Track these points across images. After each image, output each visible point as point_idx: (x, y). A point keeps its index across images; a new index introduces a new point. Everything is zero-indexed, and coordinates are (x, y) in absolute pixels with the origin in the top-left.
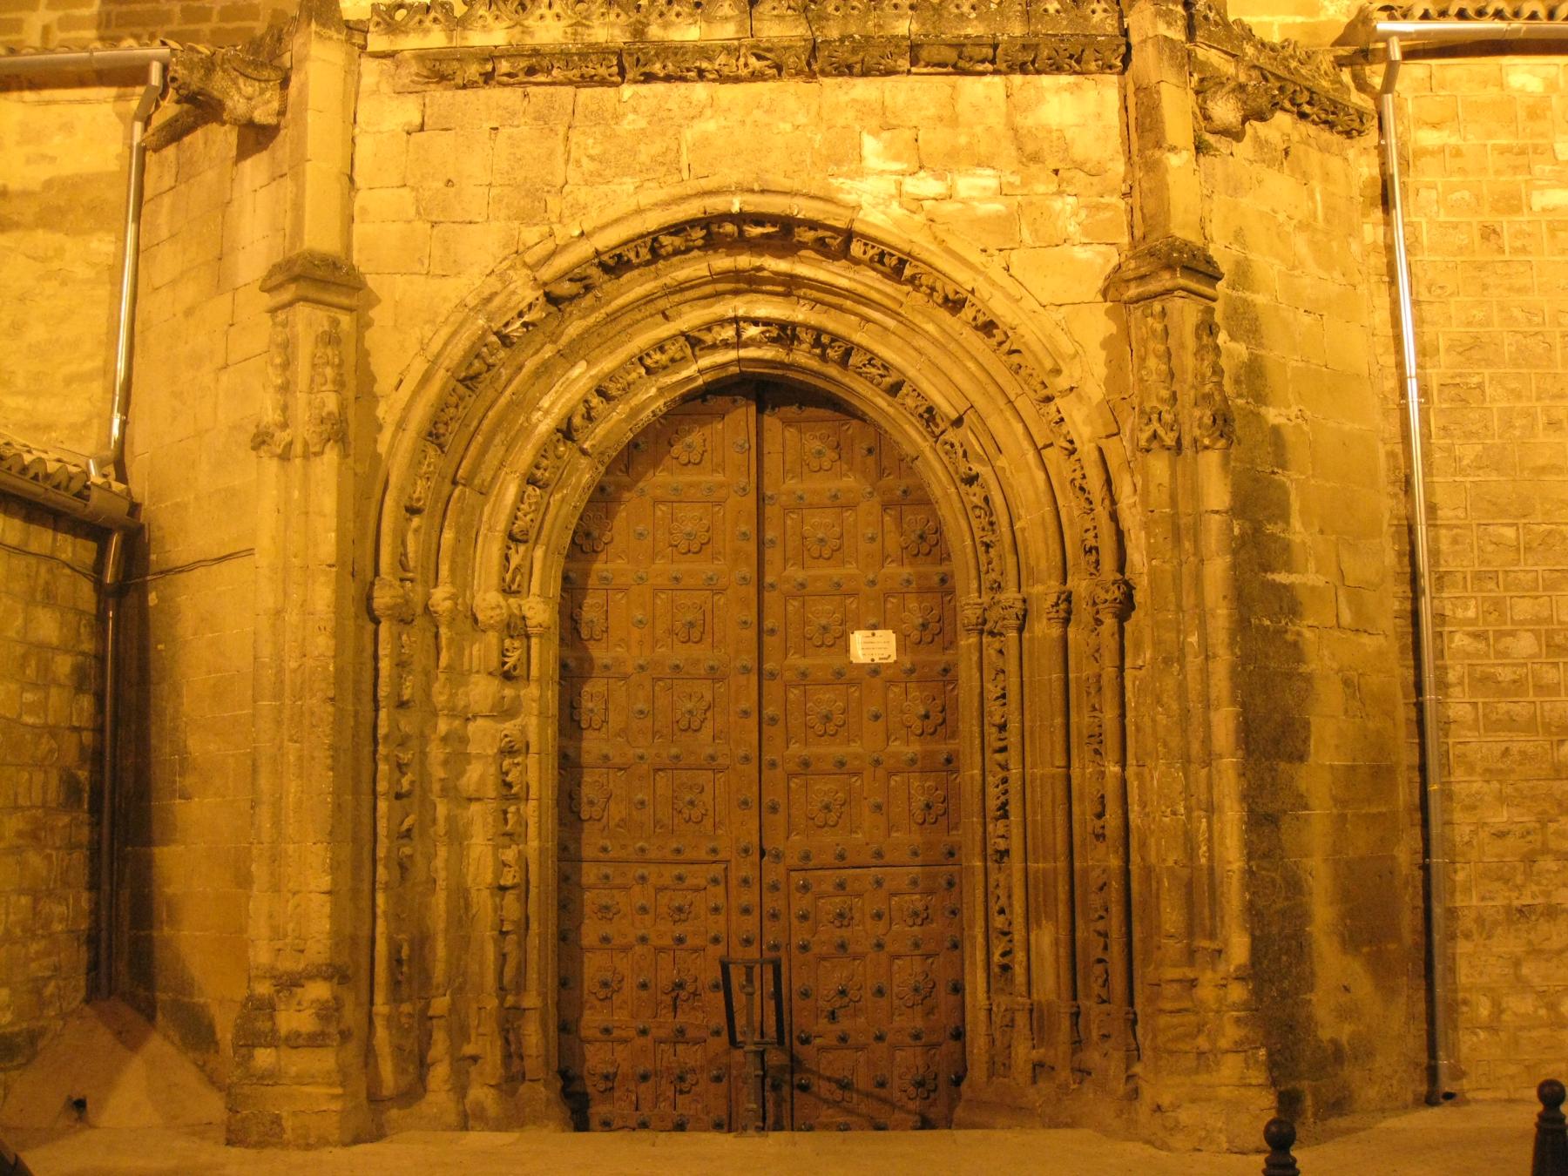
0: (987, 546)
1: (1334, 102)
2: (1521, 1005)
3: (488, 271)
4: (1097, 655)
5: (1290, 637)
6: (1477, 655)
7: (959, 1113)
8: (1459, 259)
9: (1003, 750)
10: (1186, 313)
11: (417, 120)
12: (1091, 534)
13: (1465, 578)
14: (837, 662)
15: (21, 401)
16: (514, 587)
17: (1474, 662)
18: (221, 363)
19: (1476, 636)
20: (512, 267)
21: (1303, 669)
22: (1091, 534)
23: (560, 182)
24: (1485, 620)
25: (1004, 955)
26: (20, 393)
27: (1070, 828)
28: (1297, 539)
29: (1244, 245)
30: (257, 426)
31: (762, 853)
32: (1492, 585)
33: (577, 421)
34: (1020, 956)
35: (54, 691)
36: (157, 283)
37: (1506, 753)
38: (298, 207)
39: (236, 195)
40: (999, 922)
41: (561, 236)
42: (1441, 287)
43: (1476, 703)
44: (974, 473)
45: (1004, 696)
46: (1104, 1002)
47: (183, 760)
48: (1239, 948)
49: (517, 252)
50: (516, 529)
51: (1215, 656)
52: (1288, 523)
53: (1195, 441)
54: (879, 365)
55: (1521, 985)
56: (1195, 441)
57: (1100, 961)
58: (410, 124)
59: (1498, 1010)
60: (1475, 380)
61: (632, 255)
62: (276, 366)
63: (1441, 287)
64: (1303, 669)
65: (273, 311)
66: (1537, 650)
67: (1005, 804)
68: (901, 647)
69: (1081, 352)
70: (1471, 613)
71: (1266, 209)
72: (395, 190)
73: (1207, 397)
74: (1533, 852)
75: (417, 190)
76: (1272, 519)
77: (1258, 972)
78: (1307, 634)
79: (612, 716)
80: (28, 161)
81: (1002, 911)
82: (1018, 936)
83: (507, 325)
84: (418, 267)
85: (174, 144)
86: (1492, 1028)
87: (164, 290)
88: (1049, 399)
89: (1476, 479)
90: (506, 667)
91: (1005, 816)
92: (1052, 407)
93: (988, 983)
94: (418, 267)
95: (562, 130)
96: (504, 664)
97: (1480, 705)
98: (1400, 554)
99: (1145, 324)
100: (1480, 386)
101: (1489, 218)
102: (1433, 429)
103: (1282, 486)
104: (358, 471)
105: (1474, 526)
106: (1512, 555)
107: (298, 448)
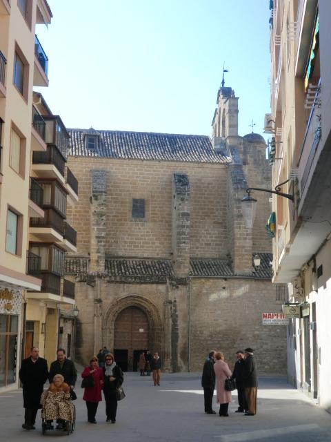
77: (173, 360)
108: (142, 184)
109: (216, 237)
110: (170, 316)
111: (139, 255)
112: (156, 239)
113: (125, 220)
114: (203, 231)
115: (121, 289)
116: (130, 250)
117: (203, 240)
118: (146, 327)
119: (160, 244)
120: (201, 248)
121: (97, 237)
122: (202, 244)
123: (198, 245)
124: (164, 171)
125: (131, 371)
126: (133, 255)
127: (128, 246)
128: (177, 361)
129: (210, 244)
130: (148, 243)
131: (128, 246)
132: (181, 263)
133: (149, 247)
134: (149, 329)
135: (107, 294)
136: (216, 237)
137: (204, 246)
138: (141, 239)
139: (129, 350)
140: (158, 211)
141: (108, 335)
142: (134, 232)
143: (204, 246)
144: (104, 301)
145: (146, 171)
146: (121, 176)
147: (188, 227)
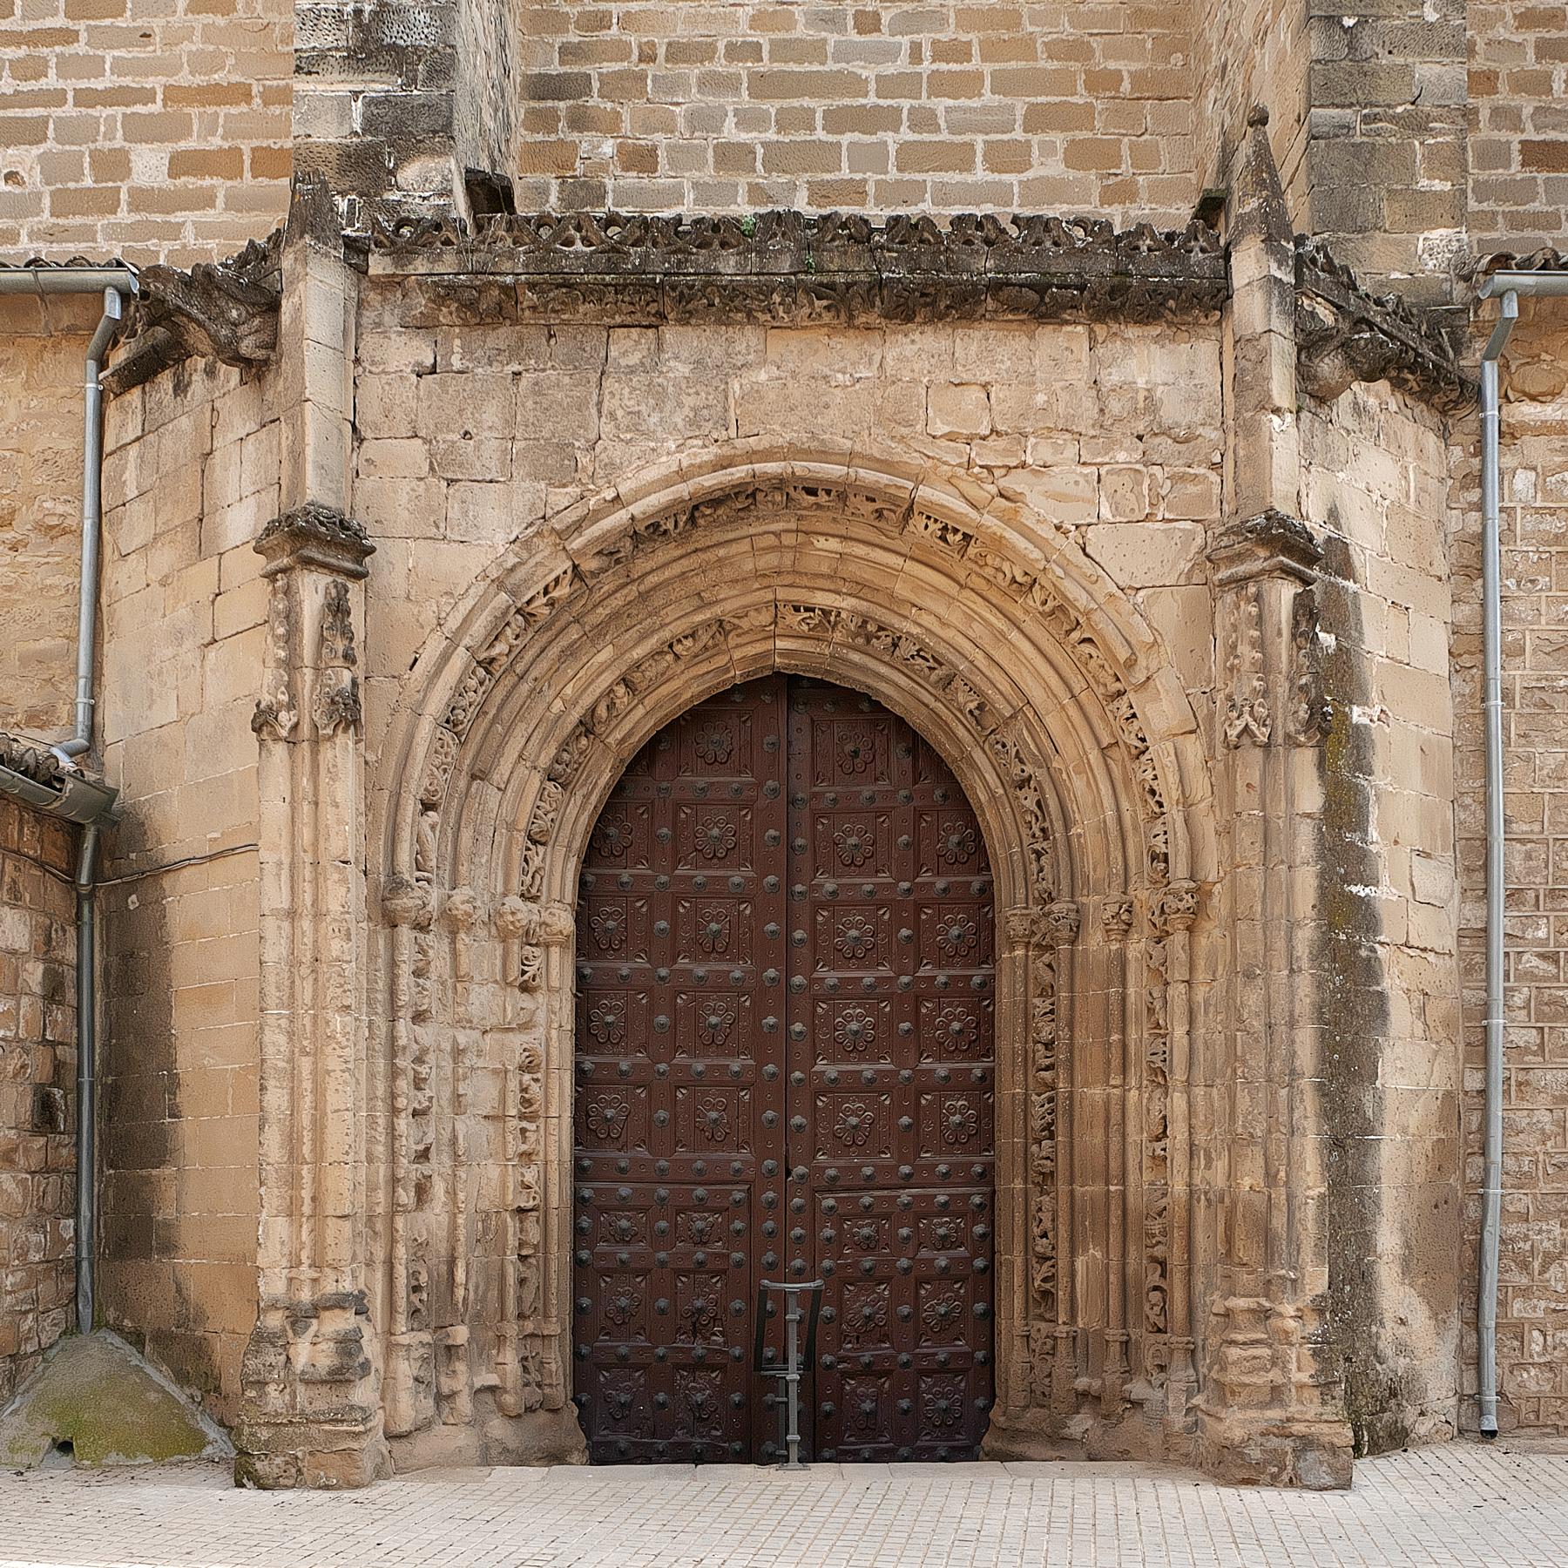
0: (1039, 854)
1: (1436, 366)
3: (512, 537)
4: (1162, 969)
5: (1363, 953)
6: (1546, 979)
7: (988, 1441)
8: (1554, 549)
10: (1285, 593)
11: (429, 362)
12: (1162, 838)
13: (1537, 897)
16: (534, 891)
17: (1542, 985)
18: (208, 639)
20: (539, 534)
22: (1162, 838)
23: (593, 436)
24: (1556, 940)
25: (1045, 1280)
27: (1072, 1160)
29: (1338, 526)
30: (258, 705)
33: (602, 711)
34: (1063, 1281)
35: (25, 1000)
38: (297, 457)
42: (1532, 581)
43: (1542, 1028)
44: (1026, 775)
45: (1052, 1012)
46: (1159, 1331)
49: (544, 517)
50: (535, 828)
51: (1300, 970)
52: (1365, 832)
53: (1288, 736)
54: (929, 657)
56: (1288, 736)
57: (1156, 1288)
58: (419, 364)
61: (670, 525)
62: (279, 637)
63: (1532, 581)
65: (271, 576)
69: (1159, 641)
70: (1541, 934)
72: (407, 441)
75: (431, 442)
81: (1044, 1235)
83: (529, 603)
85: (140, 387)
88: (1120, 694)
89: (1556, 790)
90: (526, 977)
91: (1052, 1137)
92: (1123, 703)
93: (1027, 1308)
95: (594, 378)
96: (524, 973)
97: (1546, 1030)
99: (1229, 609)
102: (1512, 735)
104: (368, 759)
105: (1551, 841)
107: (305, 730)
112: (1037, 120)
119: (1077, 156)
130: (961, 158)
138: (890, 120)
141: (483, 999)
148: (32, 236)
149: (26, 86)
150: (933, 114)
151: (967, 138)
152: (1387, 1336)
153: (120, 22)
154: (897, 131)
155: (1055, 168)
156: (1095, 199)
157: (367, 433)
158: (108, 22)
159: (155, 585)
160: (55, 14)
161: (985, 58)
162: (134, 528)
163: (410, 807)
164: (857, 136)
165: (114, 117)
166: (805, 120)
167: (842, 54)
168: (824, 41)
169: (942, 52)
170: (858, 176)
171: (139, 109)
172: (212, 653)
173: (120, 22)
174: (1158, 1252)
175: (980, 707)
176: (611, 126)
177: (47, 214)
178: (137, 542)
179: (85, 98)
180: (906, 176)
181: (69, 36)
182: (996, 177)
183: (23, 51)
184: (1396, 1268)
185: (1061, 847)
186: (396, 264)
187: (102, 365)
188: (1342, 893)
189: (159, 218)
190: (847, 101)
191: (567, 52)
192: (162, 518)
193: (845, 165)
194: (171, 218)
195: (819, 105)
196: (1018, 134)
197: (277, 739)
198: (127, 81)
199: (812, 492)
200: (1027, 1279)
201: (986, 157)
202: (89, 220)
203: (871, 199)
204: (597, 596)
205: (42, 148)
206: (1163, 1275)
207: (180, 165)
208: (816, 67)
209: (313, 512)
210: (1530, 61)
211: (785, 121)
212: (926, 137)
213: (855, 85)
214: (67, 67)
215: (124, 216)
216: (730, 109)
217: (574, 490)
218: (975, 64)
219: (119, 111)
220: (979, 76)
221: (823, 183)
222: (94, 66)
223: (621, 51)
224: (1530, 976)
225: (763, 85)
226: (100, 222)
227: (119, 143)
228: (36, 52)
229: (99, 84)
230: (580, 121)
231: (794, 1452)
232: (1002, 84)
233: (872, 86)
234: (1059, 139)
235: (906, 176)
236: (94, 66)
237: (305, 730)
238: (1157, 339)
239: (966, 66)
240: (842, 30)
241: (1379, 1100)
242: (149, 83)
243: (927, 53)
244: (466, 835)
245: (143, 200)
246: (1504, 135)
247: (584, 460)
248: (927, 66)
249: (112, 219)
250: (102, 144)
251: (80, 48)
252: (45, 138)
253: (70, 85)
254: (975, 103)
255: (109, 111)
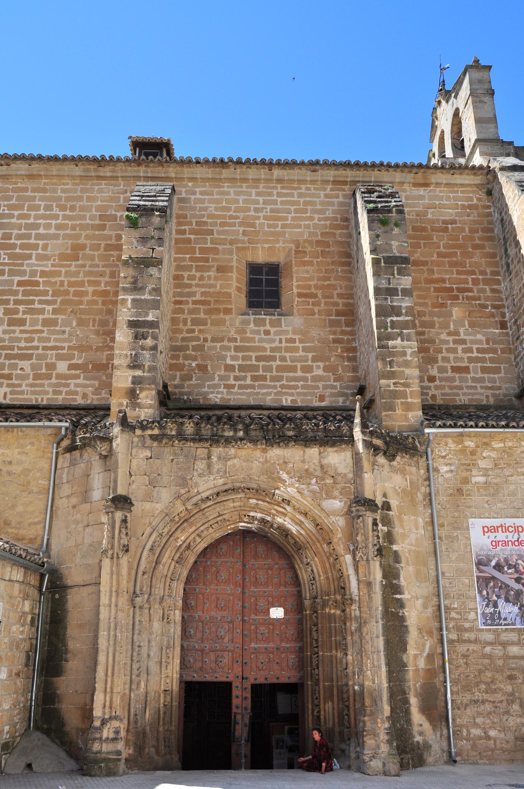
2: (476, 732)
6: (458, 619)
9: (317, 647)
11: (149, 455)
14: (266, 618)
15: (14, 531)
19: (457, 613)
21: (405, 624)
25: (317, 712)
26: (13, 528)
28: (402, 584)
31: (243, 678)
32: (462, 597)
33: (192, 544)
34: (322, 712)
36: (62, 496)
37: (468, 650)
39: (92, 473)
40: (316, 702)
41: (192, 494)
47: (66, 649)
48: (387, 710)
55: (476, 725)
59: (469, 733)
60: (456, 534)
64: (405, 624)
66: (476, 617)
67: (318, 664)
68: (285, 613)
71: (393, 486)
73: (375, 545)
74: (478, 682)
76: (395, 579)
77: (393, 718)
78: (406, 613)
79: (198, 634)
80: (19, 453)
81: (317, 698)
82: (322, 706)
84: (149, 499)
86: (467, 740)
87: (64, 499)
91: (318, 668)
94: (149, 499)
98: (434, 588)
100: (457, 536)
101: (459, 486)
103: (397, 569)
106: (468, 588)
108: (269, 226)
109: (479, 350)
110: (372, 551)
111: (269, 400)
112: (314, 359)
113: (228, 311)
114: (444, 336)
115: (201, 465)
116: (241, 387)
117: (446, 359)
118: (291, 602)
119: (326, 369)
120: (441, 379)
121: (132, 324)
122: (442, 370)
123: (434, 372)
124: (326, 196)
125: (281, 767)
126: (252, 402)
127: (236, 378)
128: (409, 721)
129: (466, 370)
130: (293, 369)
131: (236, 378)
132: (395, 395)
133: (295, 379)
134: (299, 608)
135: (153, 484)
136: (479, 350)
137: (450, 374)
138: (274, 359)
139: (236, 684)
140: (316, 287)
142: (253, 340)
143: (450, 374)
144: (138, 507)
145: (279, 195)
146: (216, 209)
147: (406, 292)
148: (27, 385)
149: (28, 345)
150: (285, 357)
151: (295, 364)
152: (416, 729)
153: (57, 328)
154: (275, 361)
155: (320, 372)
156: (332, 381)
157: (133, 473)
158: (53, 328)
159: (70, 508)
160: (38, 325)
161: (300, 343)
162: (66, 490)
163: (140, 573)
164: (264, 363)
165: (52, 354)
166: (250, 358)
167: (261, 340)
168: (255, 338)
169: (288, 341)
170: (265, 374)
171: (60, 351)
172: (87, 529)
173: (57, 328)
174: (346, 703)
175: (295, 543)
176: (195, 359)
177: (31, 379)
178: (66, 494)
179: (45, 348)
180: (278, 374)
181: (42, 332)
182: (304, 374)
183: (28, 335)
184: (417, 709)
185: (318, 583)
186: (143, 432)
187: (58, 444)
188: (393, 598)
189: (64, 381)
190: (262, 354)
191: (183, 339)
192: (74, 489)
193: (261, 370)
194: (67, 382)
195: (253, 355)
196: (310, 363)
197: (107, 557)
198: (57, 344)
199: (249, 489)
200: (313, 712)
201: (301, 369)
202: (43, 382)
203: (268, 380)
204: (191, 514)
205: (31, 362)
206: (348, 711)
207: (71, 367)
208: (253, 344)
209: (121, 496)
210: (451, 345)
211: (244, 358)
212: (284, 363)
213: (264, 349)
214: (40, 340)
215: (54, 381)
216: (228, 355)
217: (187, 490)
218: (297, 344)
219: (54, 352)
220: (298, 347)
221: (254, 376)
222: (48, 340)
223: (197, 339)
224: (454, 619)
225: (237, 349)
226: (46, 382)
227: (54, 360)
228: (31, 335)
229: (49, 345)
230: (186, 358)
231: (243, 767)
232: (305, 349)
233: (268, 350)
234: (321, 364)
235: (278, 374)
236: (48, 340)
237: (115, 555)
238: (336, 451)
239: (295, 345)
240: (260, 334)
241: (408, 657)
242: (63, 345)
243: (284, 341)
244: (154, 580)
245: (59, 376)
246: (446, 364)
247: (189, 482)
248: (284, 344)
249: (50, 381)
250: (49, 361)
251: (17, 279)
252: (32, 359)
253: (41, 345)
254: (297, 354)
255: (52, 352)
